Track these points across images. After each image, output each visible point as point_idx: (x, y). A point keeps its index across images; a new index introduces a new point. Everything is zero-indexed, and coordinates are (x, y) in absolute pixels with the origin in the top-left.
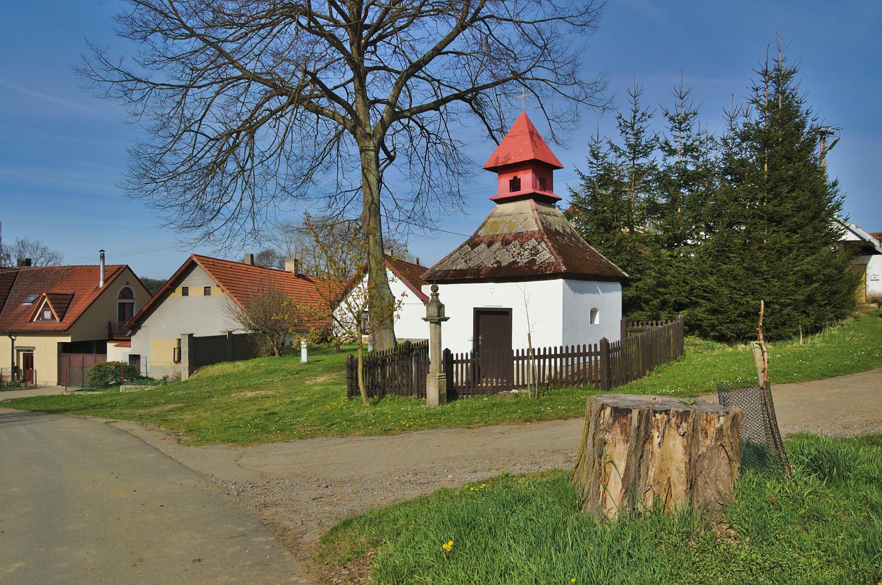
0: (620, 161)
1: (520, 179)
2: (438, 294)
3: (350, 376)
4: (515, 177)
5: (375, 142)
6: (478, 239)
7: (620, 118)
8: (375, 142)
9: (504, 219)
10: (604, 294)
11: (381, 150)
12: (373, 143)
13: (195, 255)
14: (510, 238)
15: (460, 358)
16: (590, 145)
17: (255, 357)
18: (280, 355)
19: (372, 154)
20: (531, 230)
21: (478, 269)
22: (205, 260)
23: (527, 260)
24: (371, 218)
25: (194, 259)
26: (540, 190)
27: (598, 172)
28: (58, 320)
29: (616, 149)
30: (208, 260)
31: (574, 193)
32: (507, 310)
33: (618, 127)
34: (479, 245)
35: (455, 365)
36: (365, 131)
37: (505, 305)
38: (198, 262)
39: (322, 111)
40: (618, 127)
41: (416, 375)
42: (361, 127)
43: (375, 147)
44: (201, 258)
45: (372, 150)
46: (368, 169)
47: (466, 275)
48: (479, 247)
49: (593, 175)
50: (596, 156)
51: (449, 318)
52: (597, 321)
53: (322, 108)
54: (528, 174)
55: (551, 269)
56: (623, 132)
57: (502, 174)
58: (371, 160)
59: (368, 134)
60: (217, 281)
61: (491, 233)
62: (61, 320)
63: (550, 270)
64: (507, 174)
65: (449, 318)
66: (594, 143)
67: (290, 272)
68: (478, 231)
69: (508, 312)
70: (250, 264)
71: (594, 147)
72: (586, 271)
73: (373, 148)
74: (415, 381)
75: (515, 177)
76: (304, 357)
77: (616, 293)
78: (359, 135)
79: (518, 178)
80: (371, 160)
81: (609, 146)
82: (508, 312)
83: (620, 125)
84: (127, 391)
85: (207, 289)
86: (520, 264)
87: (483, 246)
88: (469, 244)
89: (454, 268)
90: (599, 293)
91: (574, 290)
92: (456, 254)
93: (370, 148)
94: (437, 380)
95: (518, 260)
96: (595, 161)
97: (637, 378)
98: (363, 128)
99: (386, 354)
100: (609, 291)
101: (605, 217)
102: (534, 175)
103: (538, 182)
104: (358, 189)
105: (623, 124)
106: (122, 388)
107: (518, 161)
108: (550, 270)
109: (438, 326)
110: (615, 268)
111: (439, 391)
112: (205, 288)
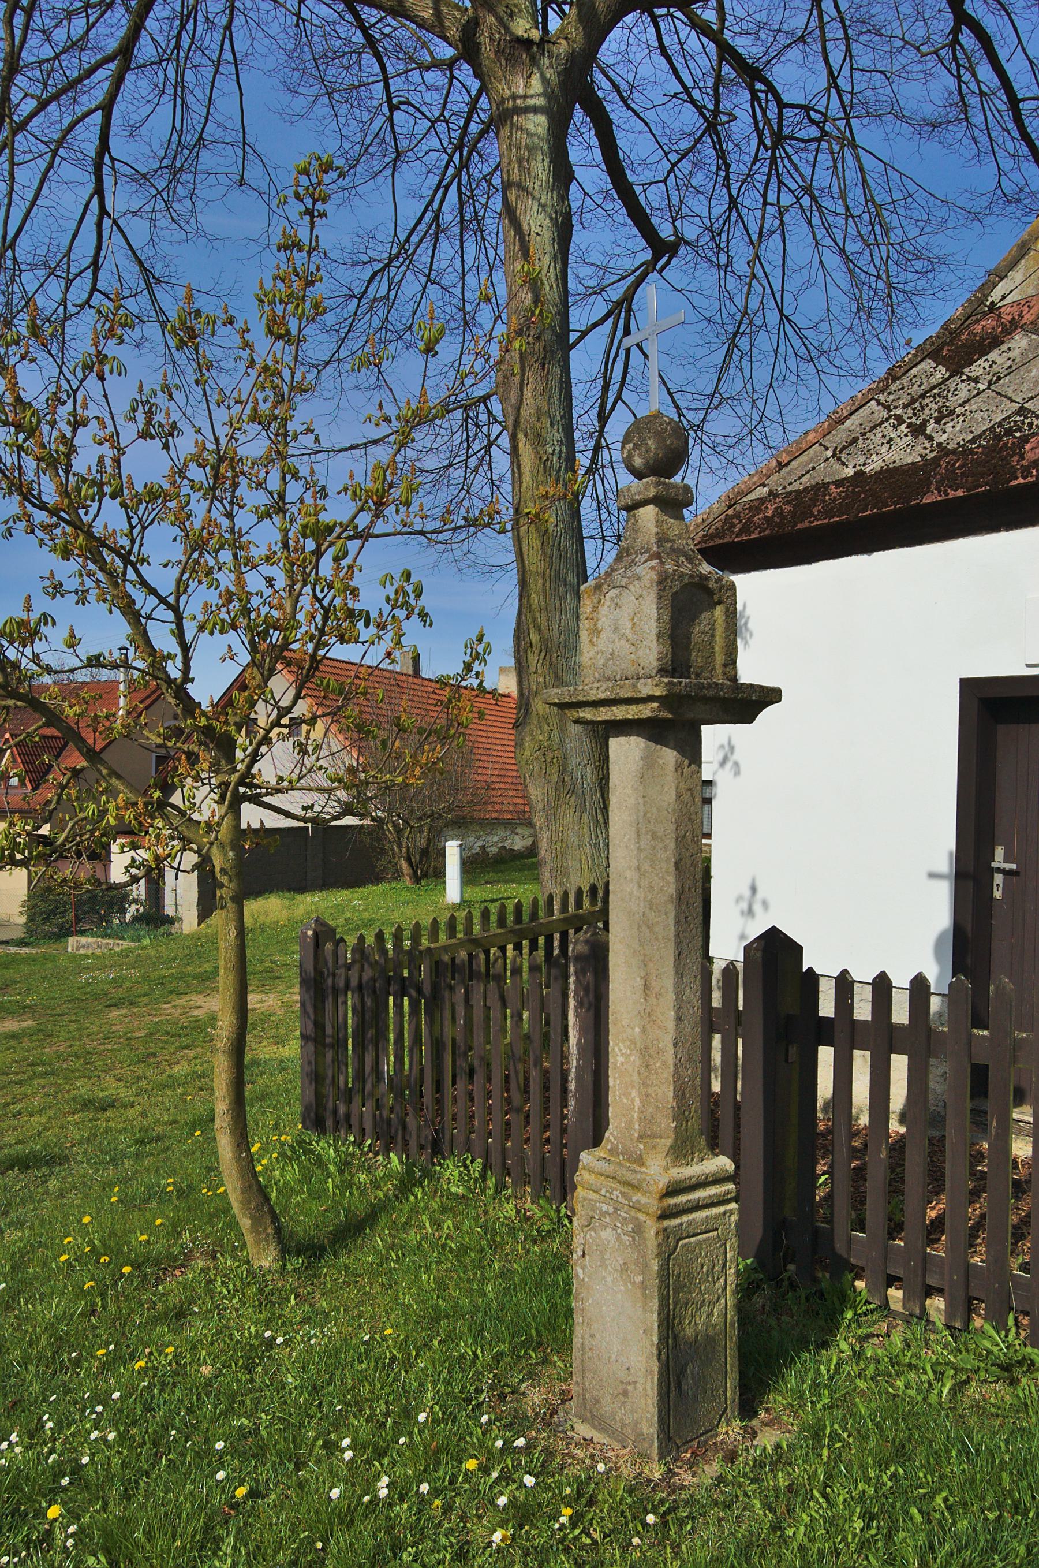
3: (310, 1029)
5: (549, 73)
6: (989, 323)
8: (549, 73)
11: (579, 114)
15: (863, 1011)
17: (377, 880)
18: (417, 880)
19: (538, 124)
21: (991, 451)
24: (530, 375)
28: (30, 788)
35: (825, 1055)
36: (507, 29)
41: (588, 1077)
42: (492, 10)
43: (548, 95)
45: (535, 110)
46: (519, 186)
47: (924, 487)
48: (993, 355)
51: (771, 696)
58: (531, 149)
59: (519, 40)
62: (34, 789)
65: (771, 696)
67: (508, 696)
68: (987, 287)
70: (411, 673)
73: (541, 102)
74: (579, 1112)
76: (453, 889)
80: (531, 149)
84: (82, 951)
89: (850, 472)
93: (531, 102)
94: (651, 1228)
99: (534, 916)
106: (72, 941)
109: (669, 756)
111: (668, 1324)
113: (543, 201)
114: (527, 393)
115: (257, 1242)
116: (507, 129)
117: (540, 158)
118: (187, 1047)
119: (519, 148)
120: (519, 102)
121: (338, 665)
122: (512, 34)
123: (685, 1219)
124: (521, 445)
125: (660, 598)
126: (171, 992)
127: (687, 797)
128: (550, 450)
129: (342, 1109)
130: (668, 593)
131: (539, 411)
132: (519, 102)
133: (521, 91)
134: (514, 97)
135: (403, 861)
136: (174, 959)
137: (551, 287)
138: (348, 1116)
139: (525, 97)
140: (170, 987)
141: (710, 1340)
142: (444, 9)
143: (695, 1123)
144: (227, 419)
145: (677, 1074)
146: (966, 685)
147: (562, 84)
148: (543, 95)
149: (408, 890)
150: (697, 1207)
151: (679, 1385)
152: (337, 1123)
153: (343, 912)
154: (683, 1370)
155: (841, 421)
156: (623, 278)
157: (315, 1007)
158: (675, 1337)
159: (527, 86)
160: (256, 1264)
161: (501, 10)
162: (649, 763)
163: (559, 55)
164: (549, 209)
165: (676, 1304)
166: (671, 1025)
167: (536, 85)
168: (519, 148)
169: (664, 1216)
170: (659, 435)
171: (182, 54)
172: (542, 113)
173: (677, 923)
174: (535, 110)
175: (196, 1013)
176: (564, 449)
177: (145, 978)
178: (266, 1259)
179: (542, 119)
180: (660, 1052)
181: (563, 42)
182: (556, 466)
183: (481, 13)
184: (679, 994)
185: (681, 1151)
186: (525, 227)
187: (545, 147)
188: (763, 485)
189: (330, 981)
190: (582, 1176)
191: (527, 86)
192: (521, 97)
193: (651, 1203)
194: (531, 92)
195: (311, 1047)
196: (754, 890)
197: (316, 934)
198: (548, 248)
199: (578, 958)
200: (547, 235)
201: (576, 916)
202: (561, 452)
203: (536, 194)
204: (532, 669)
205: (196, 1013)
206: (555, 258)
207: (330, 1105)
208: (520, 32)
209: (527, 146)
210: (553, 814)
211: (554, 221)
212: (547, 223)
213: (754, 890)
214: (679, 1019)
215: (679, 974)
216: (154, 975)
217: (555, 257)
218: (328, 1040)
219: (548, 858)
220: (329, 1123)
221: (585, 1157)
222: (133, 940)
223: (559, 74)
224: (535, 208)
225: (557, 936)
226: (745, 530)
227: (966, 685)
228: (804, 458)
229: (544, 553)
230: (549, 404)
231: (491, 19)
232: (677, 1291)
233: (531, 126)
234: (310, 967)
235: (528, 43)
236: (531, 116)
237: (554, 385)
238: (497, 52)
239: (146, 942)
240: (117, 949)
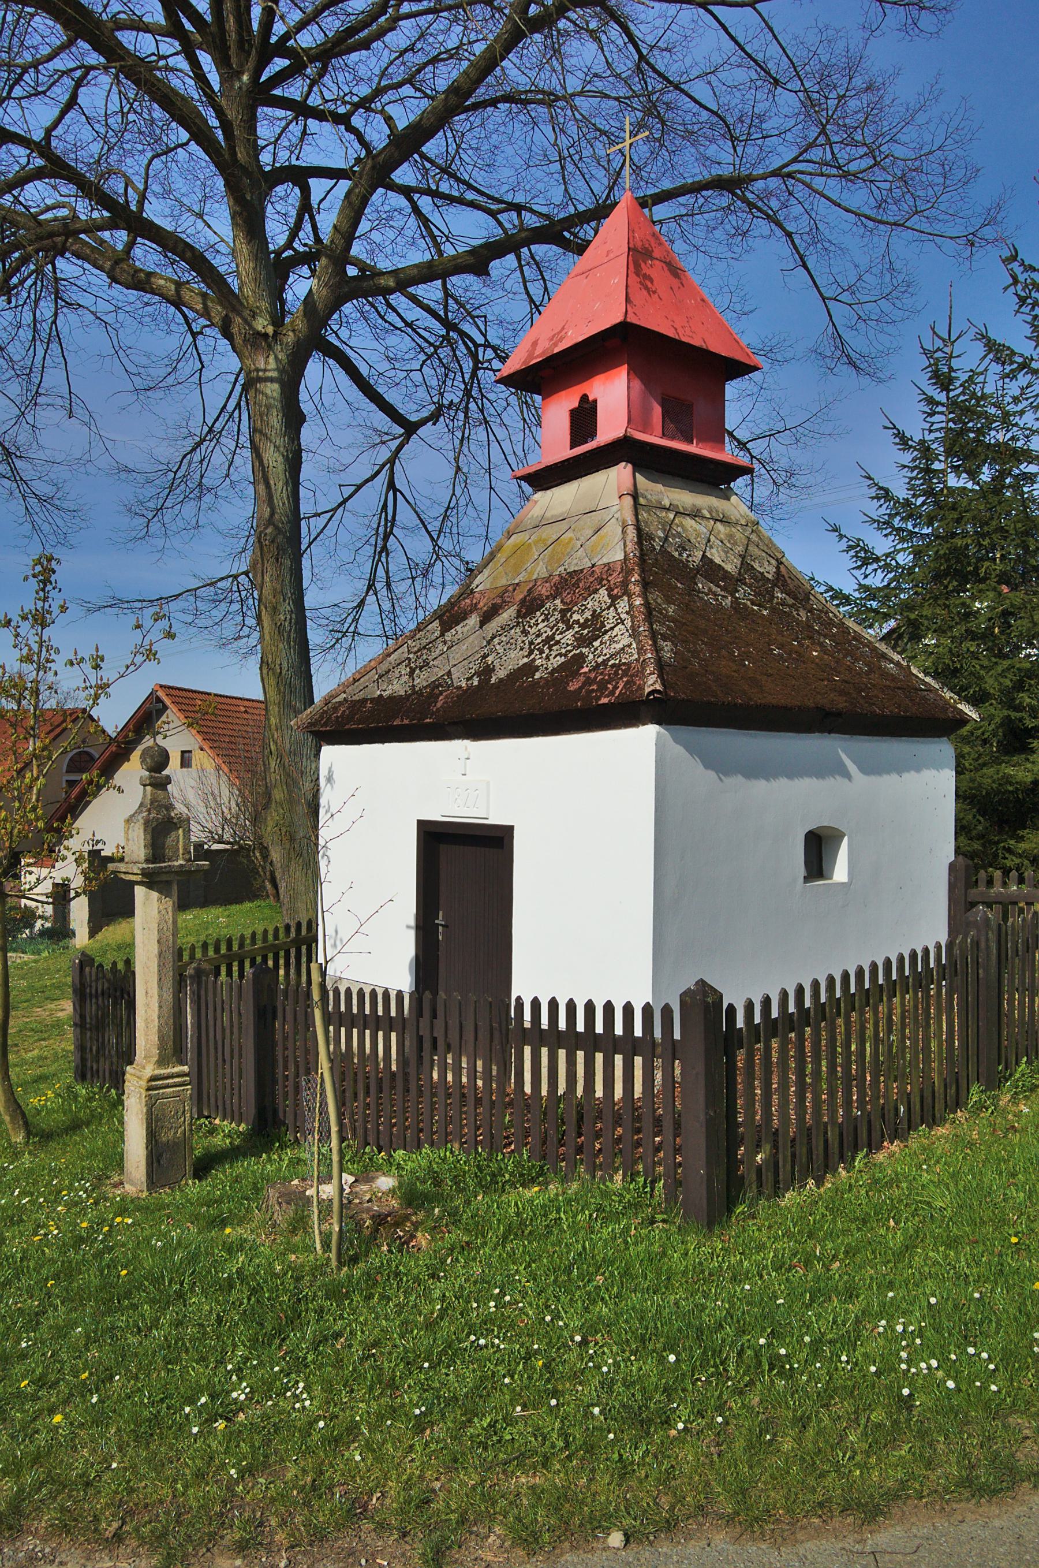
0: (1013, 388)
1: (595, 401)
2: (168, 780)
3: (78, 1021)
4: (584, 398)
7: (1014, 258)
9: (544, 536)
10: (873, 779)
12: (276, 357)
13: (161, 686)
14: (544, 590)
16: (925, 352)
20: (605, 561)
22: (184, 697)
23: (563, 659)
25: (161, 694)
26: (664, 435)
27: (951, 425)
29: (997, 351)
30: (234, 702)
31: (881, 488)
32: (498, 834)
33: (1006, 289)
34: (465, 618)
37: (496, 818)
38: (167, 701)
39: (148, 282)
40: (1006, 289)
41: (195, 1040)
42: (240, 314)
43: (281, 370)
44: (173, 692)
45: (272, 380)
46: (261, 432)
48: (458, 628)
49: (933, 436)
50: (944, 381)
52: (840, 873)
53: (150, 275)
54: (617, 382)
55: (616, 688)
56: (1022, 301)
57: (549, 396)
58: (269, 407)
59: (258, 333)
60: (199, 738)
61: (503, 582)
63: (612, 693)
64: (563, 393)
66: (939, 344)
69: (502, 839)
71: (939, 354)
72: (775, 694)
73: (275, 374)
75: (584, 398)
77: (928, 774)
78: (238, 340)
79: (591, 398)
80: (269, 407)
81: (980, 349)
82: (502, 839)
83: (1015, 281)
85: (187, 755)
86: (537, 676)
87: (473, 620)
88: (440, 618)
90: (848, 776)
91: (720, 766)
92: (400, 651)
93: (269, 374)
94: (144, 1093)
95: (538, 662)
96: (942, 397)
97: (911, 1126)
98: (245, 320)
100: (899, 768)
101: (956, 549)
102: (637, 384)
103: (657, 410)
104: (335, 510)
105: (1021, 278)
107: (580, 339)
108: (612, 693)
110: (930, 689)
112: (183, 752)
113: (277, 443)
114: (267, 578)
115: (14, 1129)
116: (253, 391)
117: (275, 414)
118: (44, 1039)
119: (260, 406)
120: (261, 374)
121: (229, 701)
122: (254, 329)
123: (161, 1091)
124: (263, 613)
125: (145, 830)
126: (47, 999)
127: (163, 912)
128: (283, 618)
129: (95, 1067)
130: (150, 829)
131: (275, 590)
132: (261, 374)
133: (262, 366)
134: (258, 370)
135: (267, 883)
136: (59, 971)
137: (284, 504)
138: (98, 1071)
139: (265, 370)
140: (47, 994)
141: (176, 1144)
142: (210, 304)
143: (170, 1050)
144: (19, 657)
145: (159, 1031)
146: (421, 823)
147: (290, 363)
148: (277, 369)
149: (271, 907)
150: (168, 1086)
151: (159, 1161)
152: (92, 1076)
153: (207, 929)
154: (161, 1155)
155: (389, 655)
156: (395, 438)
157: (80, 1006)
158: (156, 1141)
159: (266, 363)
160: (14, 1140)
161: (246, 313)
162: (147, 898)
163: (287, 343)
164: (282, 449)
165: (156, 1126)
166: (156, 1009)
167: (272, 364)
168: (260, 406)
169: (148, 1089)
170: (152, 757)
171: (33, 296)
172: (276, 382)
173: (159, 966)
174: (272, 380)
175: (60, 1014)
176: (294, 616)
177: (31, 987)
178: (19, 1138)
179: (276, 386)
180: (153, 1021)
181: (291, 333)
182: (288, 629)
183: (231, 315)
184: (160, 996)
185: (162, 1062)
186: (265, 462)
187: (279, 406)
188: (344, 692)
189: (88, 990)
190: (127, 1077)
191: (266, 363)
192: (262, 370)
193: (144, 1083)
194: (269, 367)
195: (78, 1030)
196: (336, 932)
197: (81, 961)
198: (282, 476)
199: (191, 977)
200: (281, 467)
201: (273, 945)
202: (291, 619)
203: (273, 438)
204: (272, 770)
205: (60, 1014)
206: (287, 483)
207: (89, 1064)
208: (260, 328)
209: (266, 405)
210: (286, 868)
211: (286, 458)
212: (280, 459)
213: (336, 932)
214: (160, 1007)
215: (160, 988)
216: (38, 985)
217: (287, 481)
218: (88, 1026)
219: (285, 901)
220: (89, 1076)
221: (128, 1068)
222: (33, 953)
223: (288, 356)
224: (272, 449)
225: (282, 953)
226: (325, 724)
227: (421, 823)
228: (366, 677)
229: (279, 690)
230: (282, 585)
231: (238, 320)
232: (156, 1122)
233: (269, 392)
234: (77, 982)
235: (266, 335)
236: (269, 384)
237: (286, 571)
238: (244, 341)
239: (45, 954)
240: (18, 961)
